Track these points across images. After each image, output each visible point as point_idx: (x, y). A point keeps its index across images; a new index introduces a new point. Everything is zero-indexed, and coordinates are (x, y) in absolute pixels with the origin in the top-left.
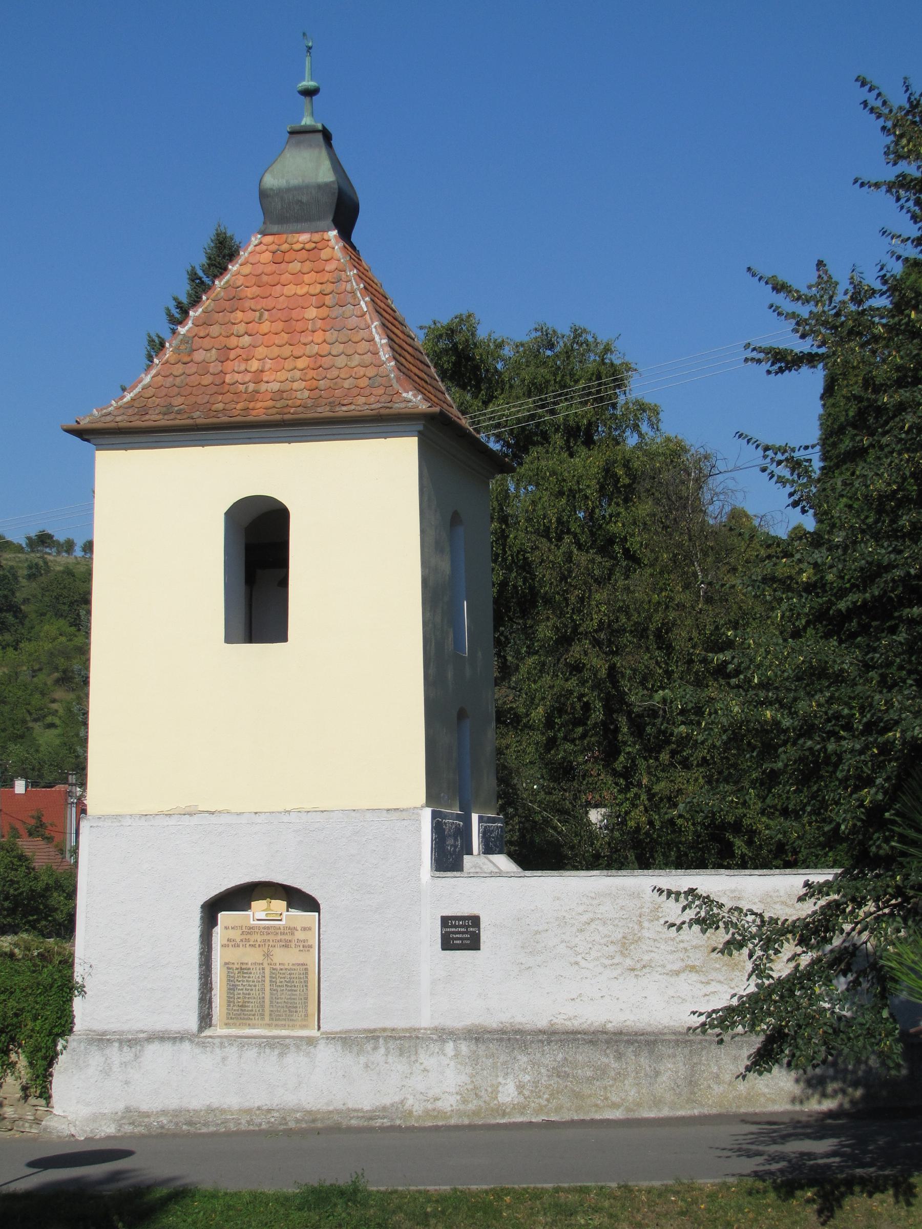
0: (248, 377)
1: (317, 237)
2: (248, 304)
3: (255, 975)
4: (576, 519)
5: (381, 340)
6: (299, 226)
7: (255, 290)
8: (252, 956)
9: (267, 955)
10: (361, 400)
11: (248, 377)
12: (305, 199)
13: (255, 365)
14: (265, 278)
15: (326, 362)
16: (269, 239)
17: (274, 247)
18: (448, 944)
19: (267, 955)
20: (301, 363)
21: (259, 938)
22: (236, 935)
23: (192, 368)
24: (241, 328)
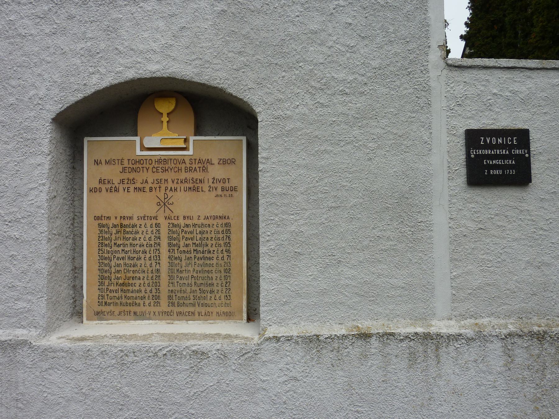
3: (144, 235)
8: (134, 206)
9: (164, 204)
19: (164, 204)
21: (151, 177)
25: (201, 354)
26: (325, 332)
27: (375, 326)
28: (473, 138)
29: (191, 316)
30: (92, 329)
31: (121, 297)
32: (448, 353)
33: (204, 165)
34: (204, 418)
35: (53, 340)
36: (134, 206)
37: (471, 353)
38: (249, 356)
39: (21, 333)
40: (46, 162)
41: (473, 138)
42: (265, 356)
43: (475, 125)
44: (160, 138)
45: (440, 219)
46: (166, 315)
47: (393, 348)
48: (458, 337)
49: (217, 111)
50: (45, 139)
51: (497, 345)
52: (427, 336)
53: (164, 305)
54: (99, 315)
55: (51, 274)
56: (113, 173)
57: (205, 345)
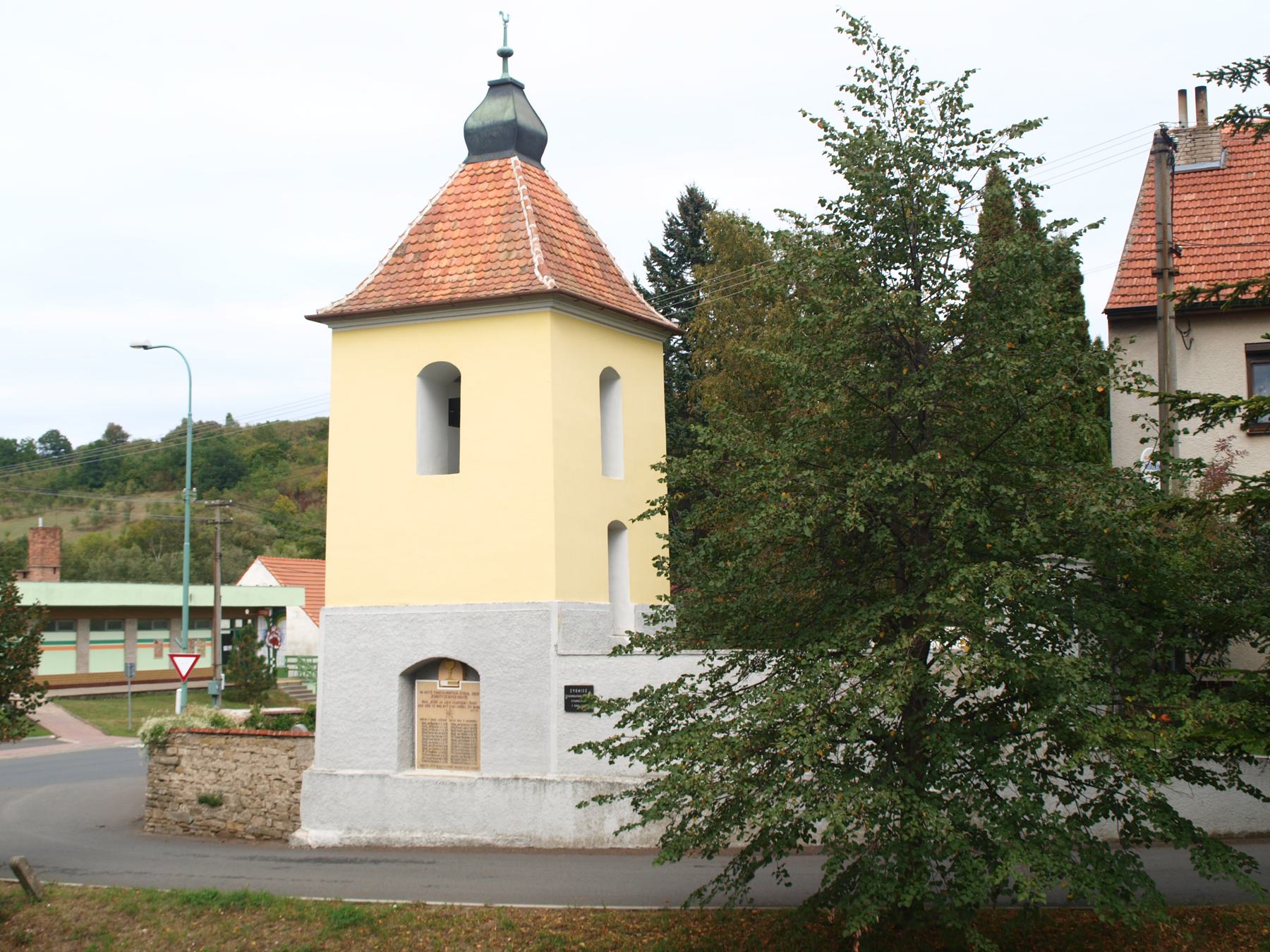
0: (439, 272)
1: (502, 162)
2: (448, 216)
3: (441, 729)
4: (1139, 506)
5: (534, 241)
6: (492, 155)
7: (454, 206)
8: (436, 714)
9: (449, 713)
10: (511, 285)
11: (439, 272)
12: (495, 134)
13: (445, 262)
14: (462, 196)
15: (493, 257)
16: (470, 166)
17: (472, 173)
18: (570, 707)
19: (449, 713)
20: (476, 259)
21: (444, 700)
22: (427, 697)
23: (403, 267)
24: (439, 236)
25: (454, 784)
26: (501, 776)
27: (522, 775)
28: (568, 689)
29: (460, 768)
30: (419, 772)
31: (432, 758)
32: (549, 788)
33: (466, 695)
34: (2, 617)
35: (400, 775)
36: (436, 714)
37: (559, 788)
38: (472, 785)
39: (386, 772)
40: (397, 694)
41: (568, 689)
42: (478, 785)
43: (569, 683)
44: (442, 683)
45: (553, 727)
46: (450, 767)
47: (528, 785)
48: (553, 781)
49: (468, 672)
50: (396, 682)
51: (570, 786)
52: (541, 780)
53: (449, 763)
54: (422, 766)
55: (400, 745)
56: (427, 697)
57: (455, 780)
